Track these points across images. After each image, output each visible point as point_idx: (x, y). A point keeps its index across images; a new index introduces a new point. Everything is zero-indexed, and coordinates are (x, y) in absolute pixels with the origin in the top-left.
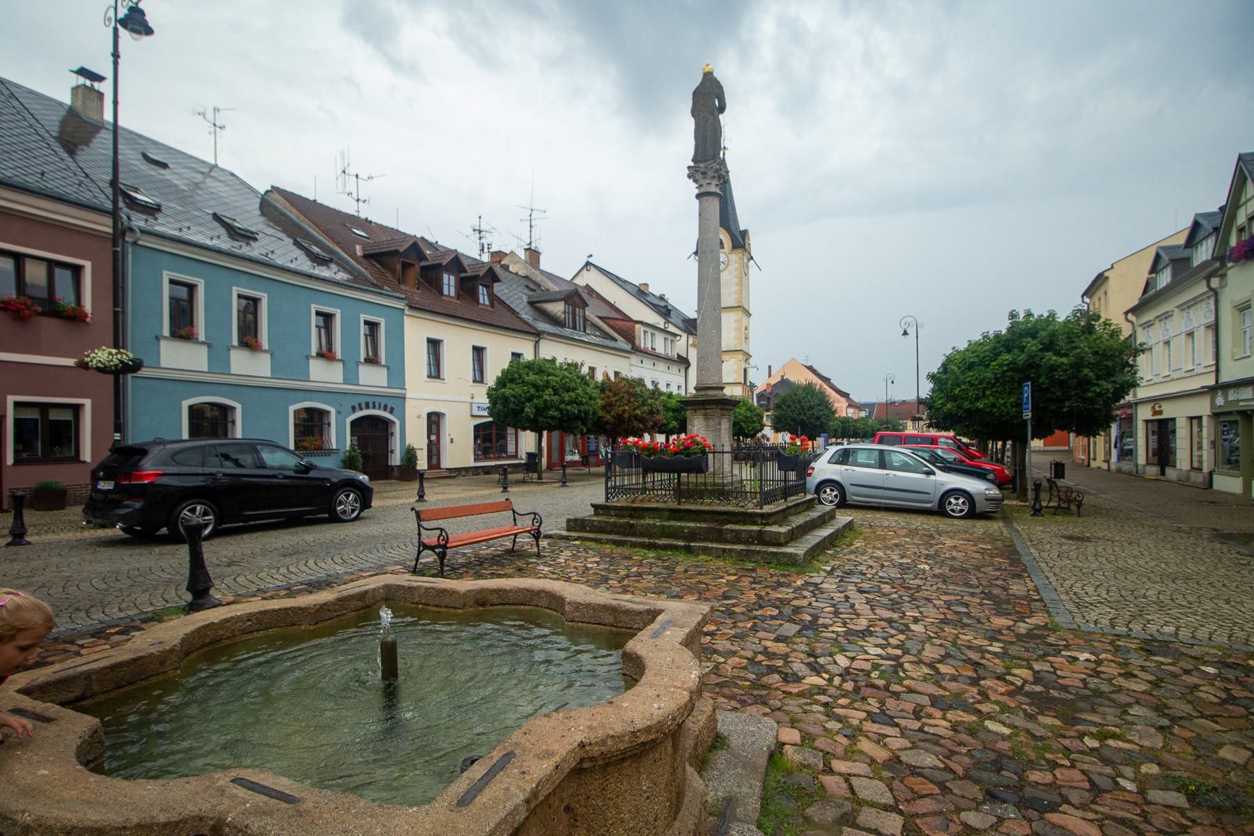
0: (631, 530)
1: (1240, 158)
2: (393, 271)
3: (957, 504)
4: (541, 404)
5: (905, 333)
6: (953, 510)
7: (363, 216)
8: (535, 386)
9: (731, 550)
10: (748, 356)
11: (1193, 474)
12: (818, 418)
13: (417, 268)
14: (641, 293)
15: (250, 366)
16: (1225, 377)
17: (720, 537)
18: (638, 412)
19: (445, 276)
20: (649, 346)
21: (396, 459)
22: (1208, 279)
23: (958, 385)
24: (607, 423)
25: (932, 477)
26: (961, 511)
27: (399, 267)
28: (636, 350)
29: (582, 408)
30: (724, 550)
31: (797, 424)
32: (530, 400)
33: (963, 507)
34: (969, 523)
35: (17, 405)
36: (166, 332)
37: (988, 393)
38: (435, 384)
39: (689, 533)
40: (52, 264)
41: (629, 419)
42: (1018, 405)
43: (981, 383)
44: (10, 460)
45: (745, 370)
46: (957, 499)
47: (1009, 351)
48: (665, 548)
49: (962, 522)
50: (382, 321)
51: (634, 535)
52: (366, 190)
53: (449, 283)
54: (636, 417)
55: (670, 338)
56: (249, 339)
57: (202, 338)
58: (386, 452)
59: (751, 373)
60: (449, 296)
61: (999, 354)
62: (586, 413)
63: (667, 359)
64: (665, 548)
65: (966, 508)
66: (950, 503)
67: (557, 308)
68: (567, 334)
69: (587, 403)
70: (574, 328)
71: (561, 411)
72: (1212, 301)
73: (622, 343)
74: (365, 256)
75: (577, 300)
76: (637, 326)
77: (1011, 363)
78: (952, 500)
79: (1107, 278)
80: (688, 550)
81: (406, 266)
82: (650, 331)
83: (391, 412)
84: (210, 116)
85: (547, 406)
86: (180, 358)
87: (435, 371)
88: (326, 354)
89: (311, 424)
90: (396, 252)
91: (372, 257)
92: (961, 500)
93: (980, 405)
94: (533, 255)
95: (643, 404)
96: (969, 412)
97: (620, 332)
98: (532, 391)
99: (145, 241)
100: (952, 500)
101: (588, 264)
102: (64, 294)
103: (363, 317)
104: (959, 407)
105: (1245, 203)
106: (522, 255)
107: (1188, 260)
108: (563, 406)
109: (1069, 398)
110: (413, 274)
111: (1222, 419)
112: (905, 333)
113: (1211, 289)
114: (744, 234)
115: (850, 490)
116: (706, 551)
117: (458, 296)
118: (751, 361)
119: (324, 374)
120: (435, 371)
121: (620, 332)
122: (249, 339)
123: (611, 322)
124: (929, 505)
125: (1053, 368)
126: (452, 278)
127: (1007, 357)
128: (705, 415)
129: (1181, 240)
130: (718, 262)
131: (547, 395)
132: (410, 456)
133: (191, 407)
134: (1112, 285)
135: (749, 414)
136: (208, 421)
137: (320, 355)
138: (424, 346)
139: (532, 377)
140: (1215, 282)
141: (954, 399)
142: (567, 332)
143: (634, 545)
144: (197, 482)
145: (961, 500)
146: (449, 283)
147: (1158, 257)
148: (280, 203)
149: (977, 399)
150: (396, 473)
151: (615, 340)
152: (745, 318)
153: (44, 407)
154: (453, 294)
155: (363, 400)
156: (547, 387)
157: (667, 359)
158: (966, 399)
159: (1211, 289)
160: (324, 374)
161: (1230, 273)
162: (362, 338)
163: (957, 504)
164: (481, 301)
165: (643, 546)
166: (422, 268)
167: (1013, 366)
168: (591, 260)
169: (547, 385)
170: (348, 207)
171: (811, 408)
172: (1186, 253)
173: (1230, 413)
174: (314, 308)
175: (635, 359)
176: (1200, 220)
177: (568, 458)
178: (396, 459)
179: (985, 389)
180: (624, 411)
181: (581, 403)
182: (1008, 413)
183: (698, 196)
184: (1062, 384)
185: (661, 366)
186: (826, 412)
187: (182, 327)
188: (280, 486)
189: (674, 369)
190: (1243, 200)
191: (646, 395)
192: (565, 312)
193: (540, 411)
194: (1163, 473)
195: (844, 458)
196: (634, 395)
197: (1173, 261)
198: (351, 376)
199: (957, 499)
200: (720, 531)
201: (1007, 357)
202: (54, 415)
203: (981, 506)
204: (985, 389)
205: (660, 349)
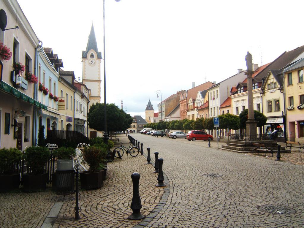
72: (261, 98)
105: (270, 79)
113: (261, 96)
190: (269, 79)
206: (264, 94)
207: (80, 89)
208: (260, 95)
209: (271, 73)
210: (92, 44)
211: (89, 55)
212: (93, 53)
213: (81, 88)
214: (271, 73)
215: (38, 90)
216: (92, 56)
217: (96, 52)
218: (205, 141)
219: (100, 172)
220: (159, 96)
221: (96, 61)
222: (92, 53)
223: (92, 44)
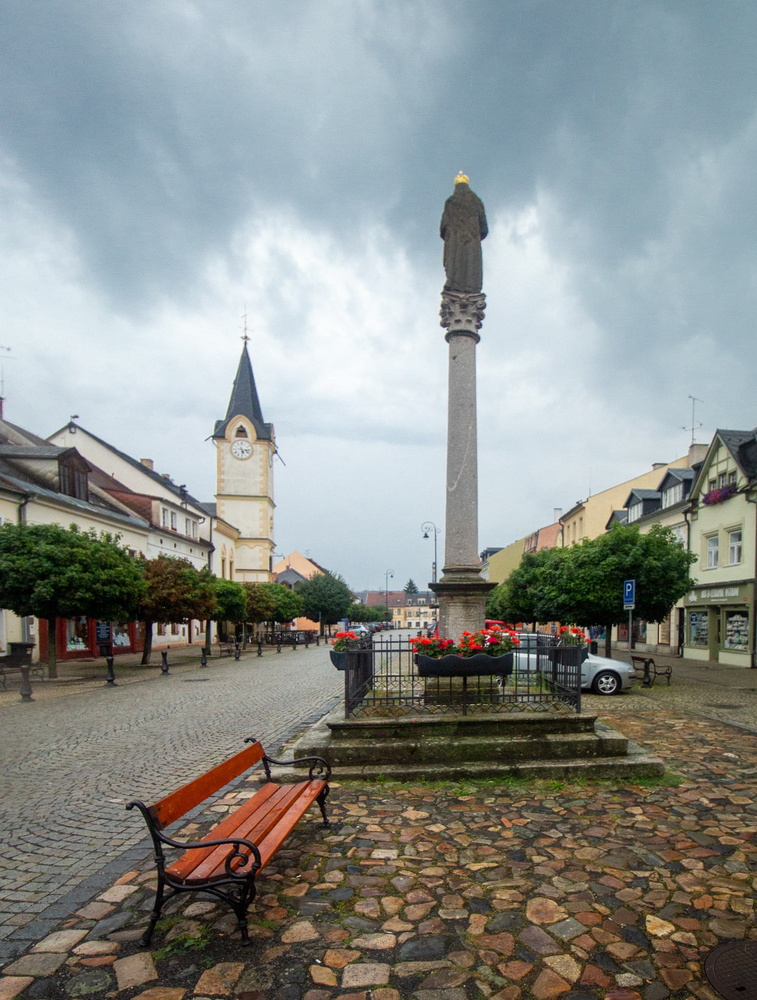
0: (413, 756)
1: (718, 432)
3: (607, 683)
4: (63, 581)
5: (426, 536)
6: (604, 689)
8: (50, 558)
9: (576, 769)
10: (273, 545)
11: (660, 647)
12: (339, 605)
14: (144, 468)
17: (548, 752)
22: (685, 513)
23: (572, 580)
24: (146, 607)
26: (611, 688)
28: (154, 528)
29: (124, 590)
30: (567, 770)
31: (319, 609)
32: (43, 576)
34: (619, 699)
39: (504, 751)
42: (620, 598)
43: (592, 579)
45: (271, 559)
46: (607, 678)
47: (614, 553)
48: (481, 775)
51: (419, 762)
54: (185, 602)
55: (192, 519)
59: (276, 561)
61: (607, 556)
62: (129, 595)
64: (481, 775)
66: (602, 682)
69: (131, 584)
71: (95, 592)
72: (687, 527)
73: (135, 517)
76: (155, 503)
77: (617, 564)
78: (603, 679)
79: (584, 508)
80: (516, 774)
82: (170, 510)
85: (73, 585)
92: (611, 680)
93: (591, 597)
96: (579, 603)
98: (47, 565)
100: (603, 679)
101: (71, 426)
105: (719, 463)
107: (658, 501)
108: (98, 586)
109: (657, 594)
111: (691, 610)
112: (426, 536)
113: (686, 520)
116: (542, 773)
118: (275, 550)
125: (651, 569)
127: (612, 559)
128: (466, 602)
129: (654, 485)
130: (59, 475)
131: (73, 571)
134: (588, 513)
135: (287, 600)
139: (43, 547)
140: (689, 516)
141: (568, 591)
143: (432, 778)
145: (611, 680)
147: (632, 496)
149: (588, 593)
151: (128, 515)
152: (270, 508)
156: (72, 562)
158: (578, 592)
159: (686, 520)
161: (700, 512)
165: (445, 776)
167: (619, 567)
168: (76, 421)
169: (72, 559)
171: (332, 596)
172: (658, 495)
173: (703, 606)
175: (153, 539)
176: (672, 473)
177: (71, 647)
181: (123, 584)
183: (448, 337)
184: (654, 582)
186: (345, 599)
190: (715, 461)
191: (197, 579)
193: (59, 591)
194: (633, 647)
196: (181, 576)
197: (645, 500)
199: (607, 678)
200: (548, 744)
201: (612, 559)
204: (596, 584)
205: (181, 530)
206: (696, 512)
207: (150, 508)
208: (683, 516)
209: (722, 442)
210: (245, 397)
211: (231, 432)
212: (245, 426)
213: (153, 509)
214: (722, 442)
215: (119, 530)
216: (241, 432)
217: (229, 421)
218: (37, 528)
219: (585, 737)
220: (431, 534)
221: (254, 446)
222: (241, 427)
223: (245, 397)
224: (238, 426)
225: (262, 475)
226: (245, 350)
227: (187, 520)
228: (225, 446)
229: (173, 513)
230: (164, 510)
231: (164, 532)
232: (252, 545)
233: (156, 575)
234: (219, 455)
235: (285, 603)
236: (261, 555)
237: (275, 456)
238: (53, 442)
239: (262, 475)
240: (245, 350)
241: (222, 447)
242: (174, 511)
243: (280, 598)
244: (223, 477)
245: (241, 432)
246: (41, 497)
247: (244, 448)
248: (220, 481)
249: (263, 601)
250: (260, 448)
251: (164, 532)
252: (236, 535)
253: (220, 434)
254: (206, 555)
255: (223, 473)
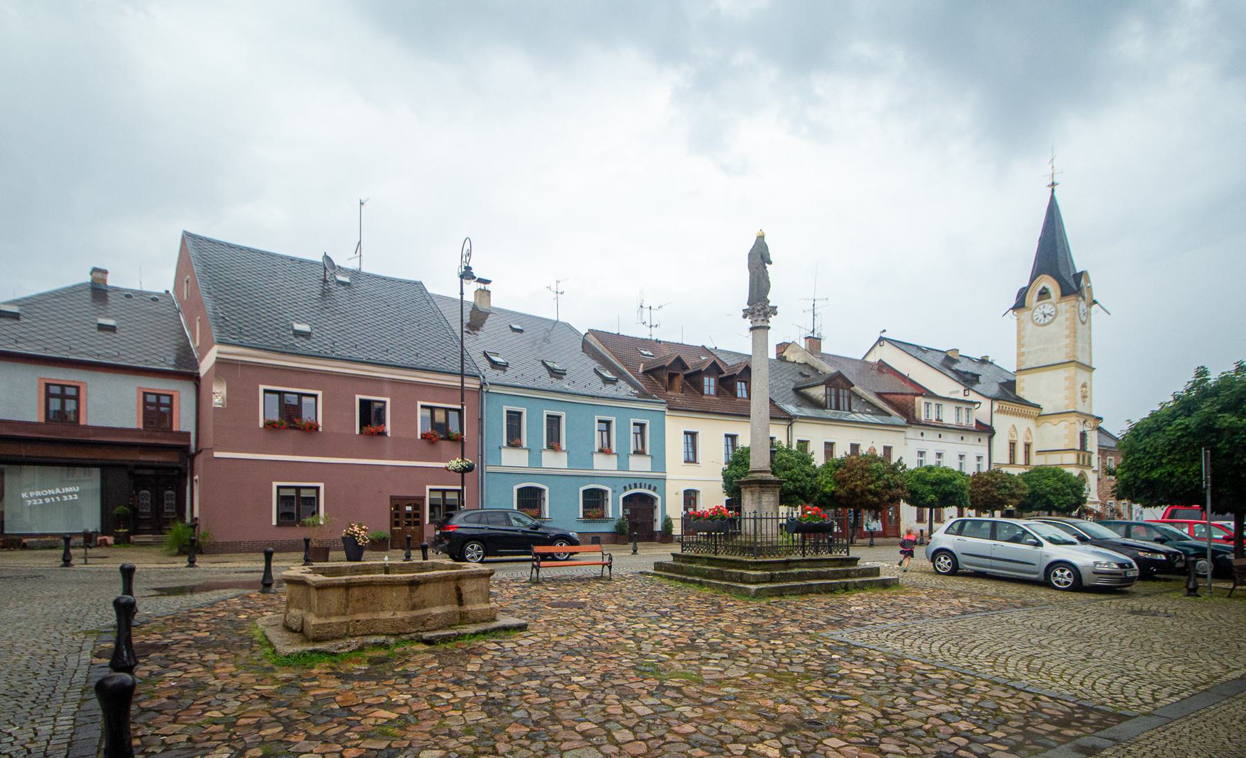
2: (662, 381)
3: (1063, 576)
7: (654, 338)
13: (681, 376)
15: (554, 461)
16: (1078, 447)
18: (872, 487)
19: (706, 379)
20: (933, 417)
21: (658, 527)
24: (840, 497)
25: (1040, 549)
26: (1066, 583)
27: (666, 378)
29: (798, 484)
33: (1068, 579)
34: (951, 579)
35: (279, 487)
36: (505, 444)
37: (1164, 461)
38: (691, 467)
40: (447, 410)
41: (862, 492)
44: (427, 521)
46: (1062, 571)
49: (1066, 594)
50: (647, 422)
52: (657, 316)
53: (709, 384)
54: (870, 491)
56: (553, 443)
57: (525, 445)
58: (652, 521)
60: (709, 395)
62: (803, 488)
63: (962, 430)
65: (1071, 580)
66: (1055, 575)
67: (818, 392)
68: (829, 416)
70: (838, 408)
73: (897, 418)
74: (645, 373)
75: (840, 381)
78: (1058, 572)
81: (672, 377)
83: (655, 490)
84: (554, 288)
86: (514, 459)
87: (692, 458)
88: (605, 451)
89: (594, 500)
90: (663, 367)
91: (652, 372)
94: (814, 342)
95: (878, 478)
96: (1147, 481)
97: (901, 404)
99: (493, 389)
100: (1058, 572)
101: (881, 339)
102: (454, 428)
103: (632, 421)
104: (1136, 477)
106: (803, 344)
110: (678, 382)
114: (1078, 277)
115: (961, 558)
117: (718, 393)
119: (604, 464)
120: (692, 458)
121: (901, 404)
122: (553, 443)
123: (891, 398)
124: (1036, 576)
126: (712, 380)
132: (668, 523)
133: (541, 491)
135: (1060, 485)
136: (530, 498)
137: (601, 451)
138: (682, 437)
142: (828, 413)
144: (476, 532)
146: (709, 384)
148: (593, 341)
149: (1153, 468)
150: (658, 537)
152: (1082, 376)
153: (298, 489)
154: (712, 392)
155: (632, 482)
157: (962, 430)
160: (604, 464)
162: (632, 436)
163: (1063, 576)
164: (739, 395)
165: (677, 579)
166: (686, 377)
168: (884, 335)
170: (643, 333)
174: (597, 418)
178: (658, 527)
179: (1162, 456)
180: (856, 486)
182: (1191, 483)
185: (950, 437)
187: (514, 440)
188: (518, 537)
189: (971, 439)
192: (826, 395)
195: (959, 529)
198: (623, 465)
199: (1062, 571)
202: (304, 494)
203: (1087, 580)
211: (1032, 298)
212: (1048, 286)
224: (1040, 288)
225: (1067, 337)
226: (1052, 198)
227: (958, 409)
228: (1025, 315)
229: (938, 406)
230: (928, 404)
231: (928, 425)
232: (1055, 420)
233: (850, 471)
234: (1019, 326)
235: (1056, 489)
236: (1066, 432)
237: (1095, 307)
238: (868, 359)
239: (1067, 337)
240: (1052, 197)
241: (1022, 318)
242: (939, 402)
243: (1050, 483)
244: (1023, 350)
245: (1044, 294)
246: (801, 417)
247: (1047, 311)
248: (1020, 355)
249: (1005, 487)
250: (1066, 306)
251: (928, 425)
252: (1034, 412)
253: (1020, 305)
254: (985, 441)
255: (1023, 346)
